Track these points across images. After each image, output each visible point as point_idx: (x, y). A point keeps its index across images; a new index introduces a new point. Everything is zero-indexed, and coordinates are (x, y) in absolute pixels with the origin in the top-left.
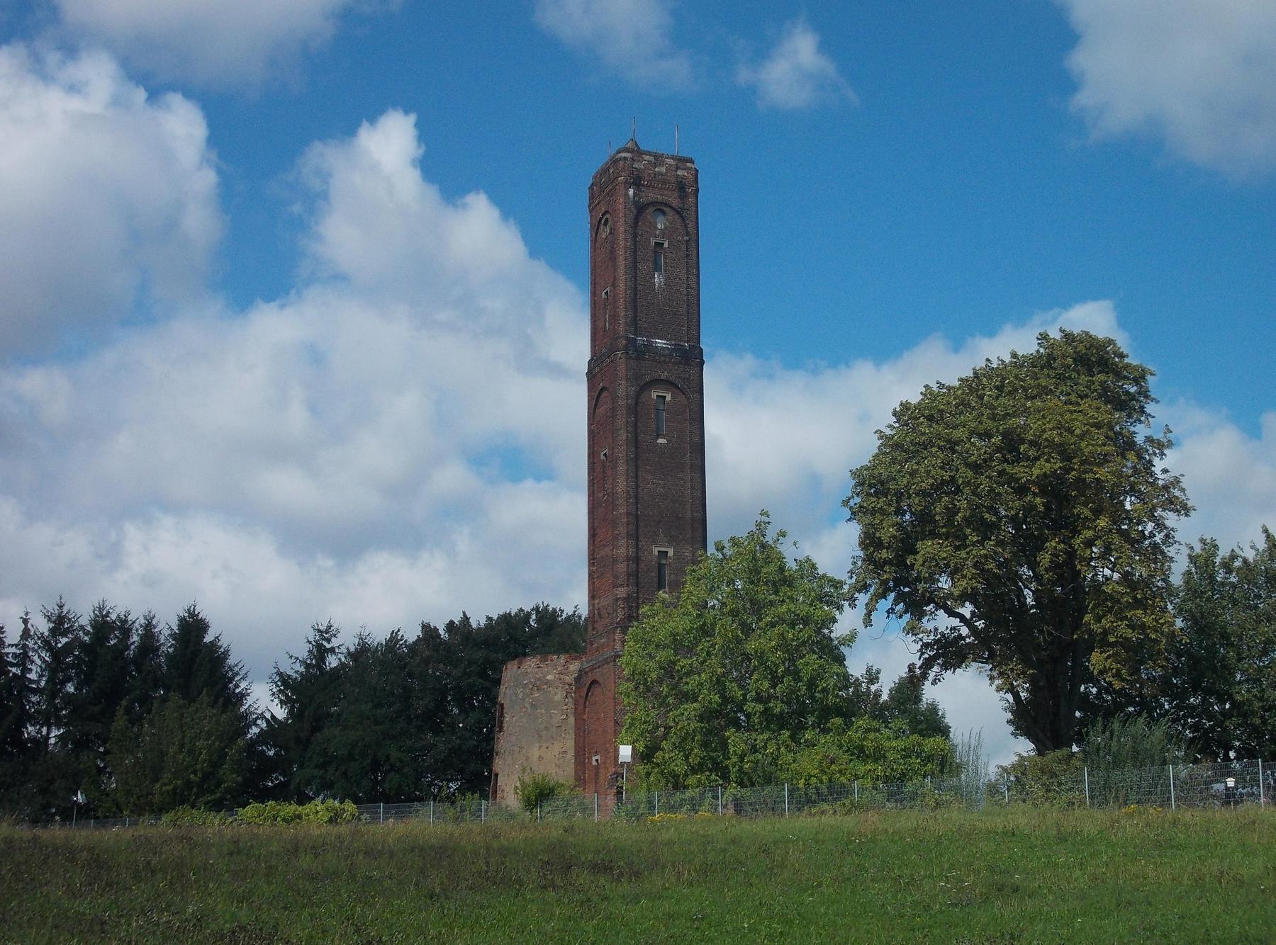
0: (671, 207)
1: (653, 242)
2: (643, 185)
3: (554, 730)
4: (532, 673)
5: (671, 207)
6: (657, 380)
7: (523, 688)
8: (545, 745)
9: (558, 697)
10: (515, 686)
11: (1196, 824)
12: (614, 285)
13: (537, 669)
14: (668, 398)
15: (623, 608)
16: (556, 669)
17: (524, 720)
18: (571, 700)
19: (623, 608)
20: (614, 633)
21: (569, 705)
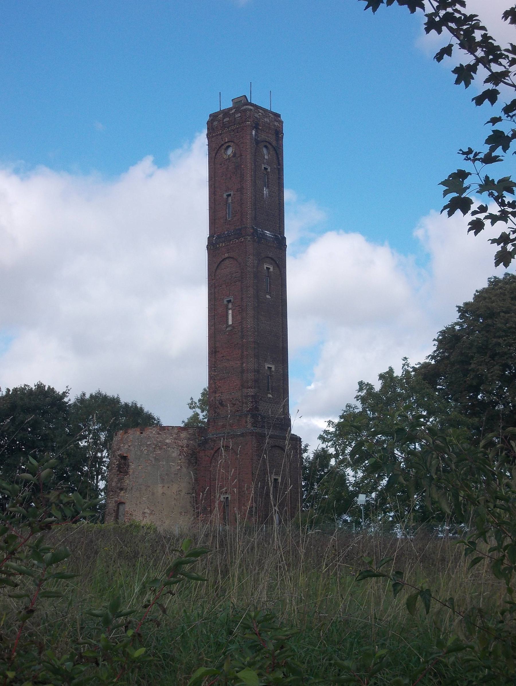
0: (272, 146)
1: (263, 166)
2: (259, 129)
3: (173, 476)
4: (154, 437)
5: (272, 146)
6: (224, 258)
7: (147, 447)
8: (166, 486)
9: (174, 455)
10: (140, 445)
11: (121, 586)
12: (241, 190)
13: (158, 435)
14: (271, 270)
15: (252, 402)
16: (172, 436)
17: (149, 468)
18: (183, 457)
19: (252, 402)
20: (247, 418)
21: (182, 460)
